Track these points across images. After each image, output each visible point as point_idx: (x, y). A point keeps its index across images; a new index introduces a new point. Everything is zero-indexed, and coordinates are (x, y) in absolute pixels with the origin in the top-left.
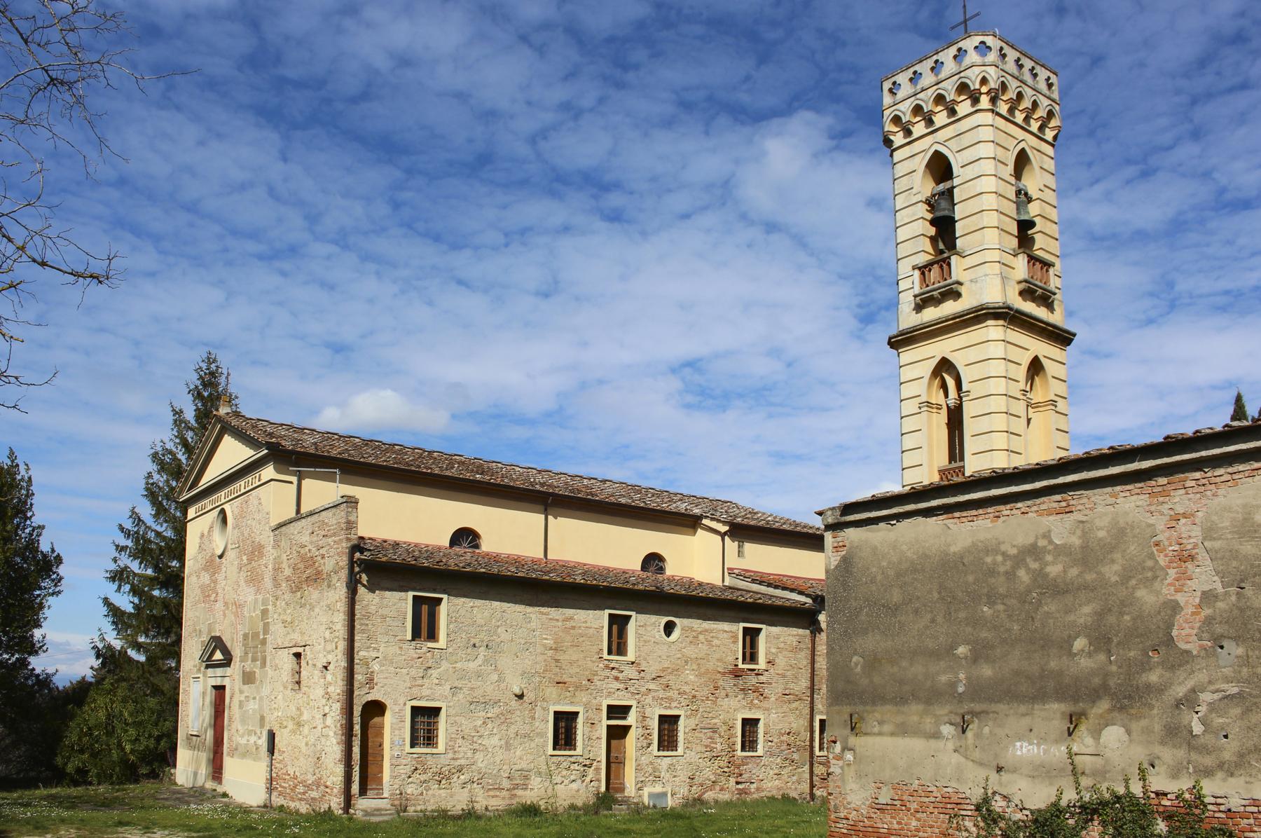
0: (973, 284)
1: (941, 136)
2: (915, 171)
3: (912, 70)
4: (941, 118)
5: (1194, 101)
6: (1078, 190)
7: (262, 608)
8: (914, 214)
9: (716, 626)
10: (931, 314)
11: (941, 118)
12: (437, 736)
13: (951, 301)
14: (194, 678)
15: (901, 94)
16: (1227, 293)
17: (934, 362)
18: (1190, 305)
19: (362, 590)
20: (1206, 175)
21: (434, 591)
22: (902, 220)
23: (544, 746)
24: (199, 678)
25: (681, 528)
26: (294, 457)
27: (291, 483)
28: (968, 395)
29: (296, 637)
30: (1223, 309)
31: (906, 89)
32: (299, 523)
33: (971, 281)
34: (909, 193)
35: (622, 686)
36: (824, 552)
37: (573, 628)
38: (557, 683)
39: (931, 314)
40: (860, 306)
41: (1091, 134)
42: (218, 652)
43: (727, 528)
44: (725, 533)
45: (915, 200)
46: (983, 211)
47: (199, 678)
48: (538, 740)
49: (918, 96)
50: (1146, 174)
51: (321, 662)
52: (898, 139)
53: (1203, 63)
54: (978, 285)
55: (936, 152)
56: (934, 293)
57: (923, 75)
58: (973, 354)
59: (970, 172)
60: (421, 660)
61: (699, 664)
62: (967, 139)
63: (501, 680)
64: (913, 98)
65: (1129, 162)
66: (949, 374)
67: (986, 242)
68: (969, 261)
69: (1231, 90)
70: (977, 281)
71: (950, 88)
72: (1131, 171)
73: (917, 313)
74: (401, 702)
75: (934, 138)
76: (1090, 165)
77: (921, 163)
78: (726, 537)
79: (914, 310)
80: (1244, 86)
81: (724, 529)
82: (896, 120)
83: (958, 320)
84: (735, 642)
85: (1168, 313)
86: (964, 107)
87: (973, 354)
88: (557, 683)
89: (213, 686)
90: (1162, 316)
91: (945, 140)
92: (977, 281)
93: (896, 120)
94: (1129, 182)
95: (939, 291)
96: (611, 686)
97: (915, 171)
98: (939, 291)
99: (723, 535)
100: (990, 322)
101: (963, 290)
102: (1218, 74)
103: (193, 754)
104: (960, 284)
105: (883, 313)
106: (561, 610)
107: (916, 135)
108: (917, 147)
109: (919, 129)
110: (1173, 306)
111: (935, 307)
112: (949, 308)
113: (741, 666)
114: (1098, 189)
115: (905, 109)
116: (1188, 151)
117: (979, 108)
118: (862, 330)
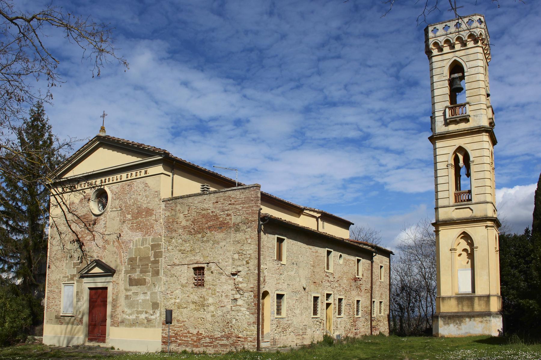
0: (475, 117)
1: (457, 54)
2: (444, 67)
3: (444, 24)
4: (458, 46)
5: (319, 60)
6: (272, 89)
7: (151, 243)
8: (443, 85)
9: (350, 258)
10: (452, 128)
11: (458, 46)
12: (281, 309)
13: (464, 123)
14: (63, 284)
15: (438, 34)
16: (324, 139)
17: (455, 148)
18: (310, 143)
19: (262, 233)
20: (322, 90)
21: (282, 235)
22: (436, 87)
23: (310, 313)
24: (74, 283)
25: (293, 213)
26: (174, 162)
27: (169, 176)
28: (473, 163)
29: (198, 258)
30: (322, 146)
31: (441, 32)
32: (200, 197)
33: (474, 116)
34: (441, 76)
35: (329, 285)
36: (348, 230)
37: (318, 256)
38: (314, 283)
39: (452, 128)
40: (173, 128)
41: (280, 66)
42: (374, 255)
43: (320, 215)
44: (319, 217)
45: (444, 79)
46: (480, 88)
47: (74, 283)
48: (309, 310)
49: (448, 36)
50: (298, 87)
51: (230, 270)
52: (435, 52)
53: (323, 45)
54: (478, 118)
55: (455, 61)
56: (457, 119)
57: (451, 27)
58: (475, 146)
59: (473, 71)
60: (279, 270)
61: (347, 275)
62: (472, 57)
63: (300, 281)
64: (445, 36)
65: (291, 80)
66: (460, 153)
67: (481, 101)
68: (472, 108)
69: (333, 58)
70: (477, 116)
71: (465, 35)
72: (293, 84)
73: (445, 126)
74: (273, 292)
75: (454, 54)
76: (277, 79)
77: (447, 65)
78: (319, 219)
79: (444, 125)
80: (339, 57)
81: (318, 215)
82: (436, 44)
83: (469, 131)
84: (355, 265)
85: (301, 145)
86: (471, 44)
87: (475, 146)
88: (314, 283)
89: (88, 288)
90: (299, 146)
91: (460, 55)
92: (477, 116)
93: (436, 44)
94: (292, 89)
95: (460, 118)
96: (327, 284)
97: (444, 67)
98: (460, 118)
99: (317, 219)
100: (484, 134)
101: (470, 119)
102: (329, 50)
103: (67, 328)
104: (469, 116)
105: (184, 132)
106: (315, 247)
107: (444, 51)
108: (445, 57)
109: (446, 49)
110: (303, 143)
111: (465, 123)
112: (462, 126)
113: (357, 276)
114: (280, 90)
115: (441, 40)
116: (315, 80)
117: (478, 45)
118: (173, 139)
